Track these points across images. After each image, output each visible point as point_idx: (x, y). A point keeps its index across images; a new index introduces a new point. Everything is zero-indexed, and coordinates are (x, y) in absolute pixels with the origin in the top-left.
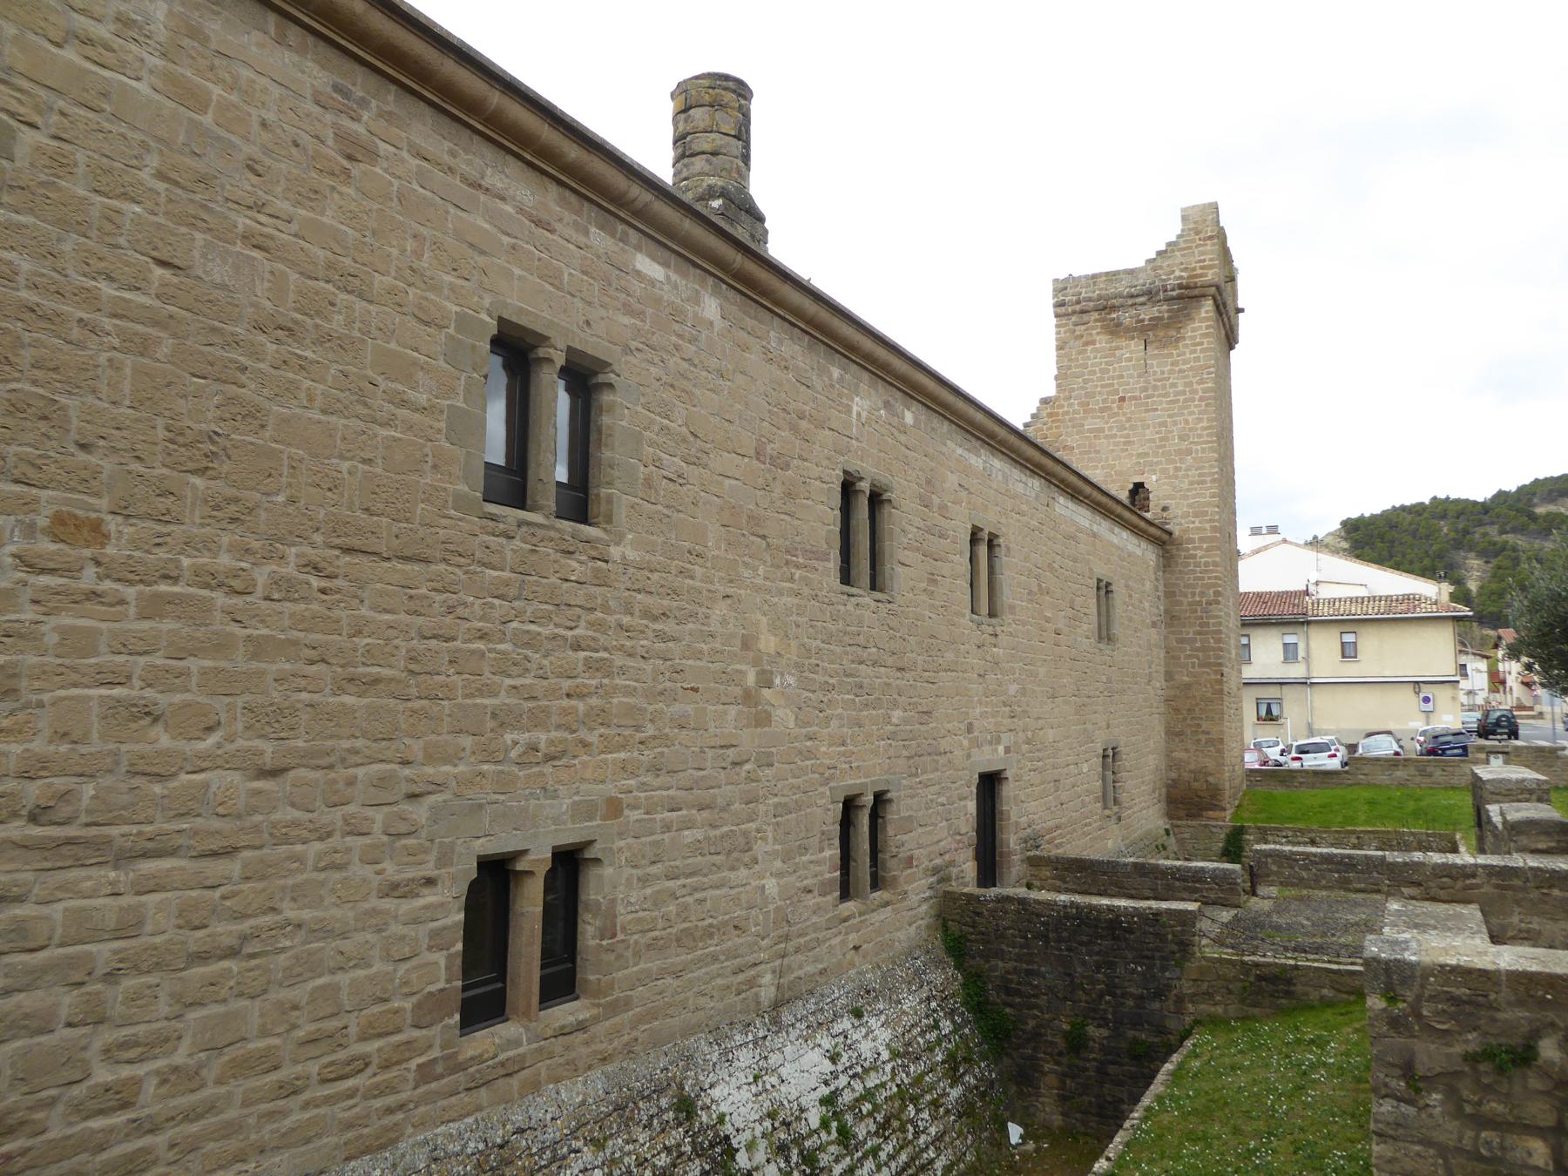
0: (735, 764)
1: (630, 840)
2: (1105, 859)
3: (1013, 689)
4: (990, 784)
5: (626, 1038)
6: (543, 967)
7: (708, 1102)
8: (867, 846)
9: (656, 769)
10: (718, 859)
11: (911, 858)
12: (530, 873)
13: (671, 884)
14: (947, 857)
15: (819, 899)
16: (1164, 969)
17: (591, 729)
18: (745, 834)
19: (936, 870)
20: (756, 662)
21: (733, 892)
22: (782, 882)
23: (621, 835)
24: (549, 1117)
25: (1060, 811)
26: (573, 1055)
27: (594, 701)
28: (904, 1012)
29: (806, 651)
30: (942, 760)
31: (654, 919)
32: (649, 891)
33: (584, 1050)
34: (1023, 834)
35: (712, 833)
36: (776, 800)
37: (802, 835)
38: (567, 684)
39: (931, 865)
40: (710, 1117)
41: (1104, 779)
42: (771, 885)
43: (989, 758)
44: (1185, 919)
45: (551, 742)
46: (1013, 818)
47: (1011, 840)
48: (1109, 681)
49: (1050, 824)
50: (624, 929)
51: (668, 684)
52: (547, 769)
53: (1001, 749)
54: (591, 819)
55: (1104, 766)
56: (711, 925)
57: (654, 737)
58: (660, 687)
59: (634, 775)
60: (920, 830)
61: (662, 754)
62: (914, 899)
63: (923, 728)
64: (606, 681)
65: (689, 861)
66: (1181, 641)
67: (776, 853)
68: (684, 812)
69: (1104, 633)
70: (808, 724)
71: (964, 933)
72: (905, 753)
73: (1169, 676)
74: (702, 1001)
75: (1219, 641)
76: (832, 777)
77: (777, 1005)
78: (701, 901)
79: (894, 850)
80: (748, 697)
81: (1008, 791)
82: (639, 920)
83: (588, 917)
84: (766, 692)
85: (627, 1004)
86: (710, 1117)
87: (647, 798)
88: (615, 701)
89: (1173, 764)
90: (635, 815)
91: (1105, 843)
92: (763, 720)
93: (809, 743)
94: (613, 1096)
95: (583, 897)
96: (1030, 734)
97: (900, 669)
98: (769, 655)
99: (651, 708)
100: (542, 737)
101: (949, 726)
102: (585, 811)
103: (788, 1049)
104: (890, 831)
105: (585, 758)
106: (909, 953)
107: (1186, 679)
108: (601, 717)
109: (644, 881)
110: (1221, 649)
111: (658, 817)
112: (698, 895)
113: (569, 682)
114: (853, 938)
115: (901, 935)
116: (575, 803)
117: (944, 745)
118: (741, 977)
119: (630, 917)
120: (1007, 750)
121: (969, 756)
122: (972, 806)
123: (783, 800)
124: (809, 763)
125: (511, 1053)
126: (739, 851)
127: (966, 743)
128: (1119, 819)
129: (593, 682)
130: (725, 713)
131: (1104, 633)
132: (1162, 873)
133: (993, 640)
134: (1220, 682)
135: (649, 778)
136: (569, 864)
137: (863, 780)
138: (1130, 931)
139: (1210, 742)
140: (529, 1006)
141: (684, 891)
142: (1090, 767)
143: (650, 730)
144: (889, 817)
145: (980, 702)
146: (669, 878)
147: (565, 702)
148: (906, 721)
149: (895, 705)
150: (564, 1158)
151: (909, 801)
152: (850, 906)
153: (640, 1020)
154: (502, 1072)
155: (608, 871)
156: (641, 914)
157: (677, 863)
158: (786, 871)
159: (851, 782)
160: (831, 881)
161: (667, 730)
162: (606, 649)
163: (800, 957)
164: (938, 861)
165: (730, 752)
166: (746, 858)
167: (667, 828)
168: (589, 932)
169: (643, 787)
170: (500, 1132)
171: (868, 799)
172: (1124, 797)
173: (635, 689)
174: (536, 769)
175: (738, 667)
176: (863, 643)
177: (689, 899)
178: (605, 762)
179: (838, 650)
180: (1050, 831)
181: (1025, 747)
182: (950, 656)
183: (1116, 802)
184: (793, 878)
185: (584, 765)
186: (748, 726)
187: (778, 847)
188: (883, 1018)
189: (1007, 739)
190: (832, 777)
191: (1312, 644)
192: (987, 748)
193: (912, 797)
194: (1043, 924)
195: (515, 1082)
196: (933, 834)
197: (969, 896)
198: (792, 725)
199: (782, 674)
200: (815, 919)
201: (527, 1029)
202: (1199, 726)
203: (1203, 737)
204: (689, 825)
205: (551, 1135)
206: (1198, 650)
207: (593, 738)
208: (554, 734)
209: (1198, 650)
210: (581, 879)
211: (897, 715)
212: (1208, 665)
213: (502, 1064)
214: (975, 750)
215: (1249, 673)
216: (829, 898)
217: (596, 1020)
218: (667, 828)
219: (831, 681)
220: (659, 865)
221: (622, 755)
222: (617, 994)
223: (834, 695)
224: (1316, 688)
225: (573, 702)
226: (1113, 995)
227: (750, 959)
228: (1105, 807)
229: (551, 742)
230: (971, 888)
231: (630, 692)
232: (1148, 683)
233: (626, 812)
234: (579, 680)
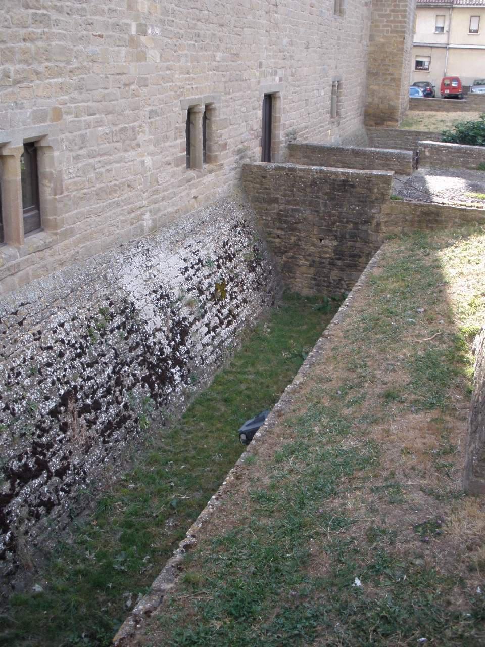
0: (126, 85)
1: (68, 134)
2: (328, 145)
3: (285, 41)
4: (270, 99)
5: (72, 252)
6: (25, 212)
7: (120, 285)
8: (201, 137)
9: (80, 88)
10: (118, 145)
11: (226, 144)
12: (12, 156)
13: (92, 161)
14: (245, 144)
15: (175, 169)
16: (371, 208)
17: (40, 63)
18: (133, 129)
19: (240, 151)
20: (137, 18)
21: (127, 165)
22: (154, 158)
23: (62, 131)
24: (37, 297)
25: (310, 120)
26: (45, 262)
27: (40, 44)
28: (223, 234)
29: (165, 12)
30: (244, 85)
31: (84, 182)
32: (80, 165)
33: (51, 259)
34: (287, 131)
35: (114, 129)
36: (150, 108)
37: (165, 129)
38: (23, 32)
39: (236, 149)
40: (122, 293)
41: (332, 99)
42: (148, 160)
43: (271, 84)
44: (386, 180)
45: (17, 72)
46: (282, 122)
47: (281, 136)
48: (339, 39)
49: (302, 125)
50: (67, 189)
51: (85, 33)
52: (16, 89)
53: (277, 78)
54: (44, 121)
55: (333, 92)
56: (115, 185)
57: (78, 68)
58: (80, 35)
59: (67, 93)
60: (231, 127)
61: (83, 79)
62: (226, 168)
63: (233, 64)
64: (46, 30)
65: (102, 146)
66: (382, 16)
67: (150, 140)
68: (97, 116)
69: (338, 8)
70: (167, 60)
71: (257, 186)
72: (224, 80)
73: (372, 38)
74: (112, 229)
75: (404, 17)
76: (182, 94)
77: (154, 229)
78: (108, 171)
79: (216, 139)
80: (132, 42)
81: (280, 104)
82: (75, 183)
83: (46, 182)
84: (142, 38)
85: (71, 232)
86: (122, 293)
87: (76, 107)
88: (53, 44)
89: (368, 91)
90: (70, 118)
91: (330, 137)
92: (141, 57)
93: (168, 72)
94: (69, 284)
95: (41, 170)
96: (293, 70)
97: (221, 25)
98: (144, 13)
99: (75, 48)
100: (11, 68)
101: (248, 63)
102: (40, 116)
103: (161, 256)
104: (214, 128)
105: (38, 82)
106: (224, 200)
107: (382, 40)
108: (47, 54)
109: (77, 158)
110: (405, 22)
111: (83, 119)
112: (108, 167)
113: (25, 31)
114: (194, 192)
115: (219, 190)
116: (34, 112)
117: (245, 75)
118: (133, 215)
119: (70, 181)
120: (281, 80)
121: (259, 82)
122: (260, 113)
123: (154, 108)
124: (168, 84)
125: (13, 263)
126: (127, 138)
127: (258, 74)
128: (339, 124)
129: (40, 31)
130: (119, 52)
131: (338, 8)
132: (364, 154)
133: (275, 9)
134: (403, 43)
135: (75, 94)
136: (32, 149)
137: (198, 97)
138: (353, 186)
139: (393, 80)
140: (18, 235)
141: (99, 165)
142: (325, 92)
143: (75, 64)
144: (213, 119)
145: (266, 48)
146: (90, 157)
147: (22, 45)
148: (224, 59)
149: (218, 48)
150: (48, 317)
151: (225, 109)
152: (192, 173)
153: (79, 241)
154: (9, 273)
155: (56, 154)
156: (76, 179)
157: (95, 148)
158: (155, 154)
159: (193, 97)
160: (182, 157)
161: (85, 63)
162: (45, 8)
163: (165, 203)
164: (241, 146)
165: (123, 77)
166: (134, 144)
167: (88, 126)
168: (47, 191)
169: (73, 100)
170: (13, 306)
171: (202, 108)
172: (342, 111)
173: (65, 35)
174: (10, 90)
175: (126, 21)
176: (199, 6)
177: (103, 170)
178: (49, 84)
179: (185, 11)
180: (302, 129)
181: (290, 78)
182: (250, 17)
183: (338, 114)
184: (159, 157)
185: (38, 86)
186: (132, 61)
187: (151, 137)
188: (211, 237)
189: (281, 72)
190: (182, 94)
191: (453, 23)
192: (269, 78)
193: (227, 107)
194: (303, 182)
195: (16, 279)
196: (238, 132)
197: (258, 167)
198: (158, 61)
199: (152, 27)
200: (172, 180)
201: (19, 249)
202: (387, 70)
203: (389, 78)
204: (100, 123)
205: (39, 306)
206: (391, 22)
207: (41, 69)
208: (18, 66)
209: (391, 22)
210: (39, 159)
211: (219, 55)
212: (397, 32)
213: (8, 269)
214: (262, 79)
215: (417, 39)
216: (180, 168)
217: (56, 242)
218: (88, 126)
219: (181, 32)
220: (85, 149)
221: (60, 80)
222: (66, 227)
223: (182, 41)
224: (451, 50)
225: (28, 44)
226: (341, 222)
227: (138, 204)
228: (332, 117)
229: (17, 72)
230: (258, 163)
231: (63, 37)
232: (360, 42)
233: (64, 116)
234: (30, 30)
